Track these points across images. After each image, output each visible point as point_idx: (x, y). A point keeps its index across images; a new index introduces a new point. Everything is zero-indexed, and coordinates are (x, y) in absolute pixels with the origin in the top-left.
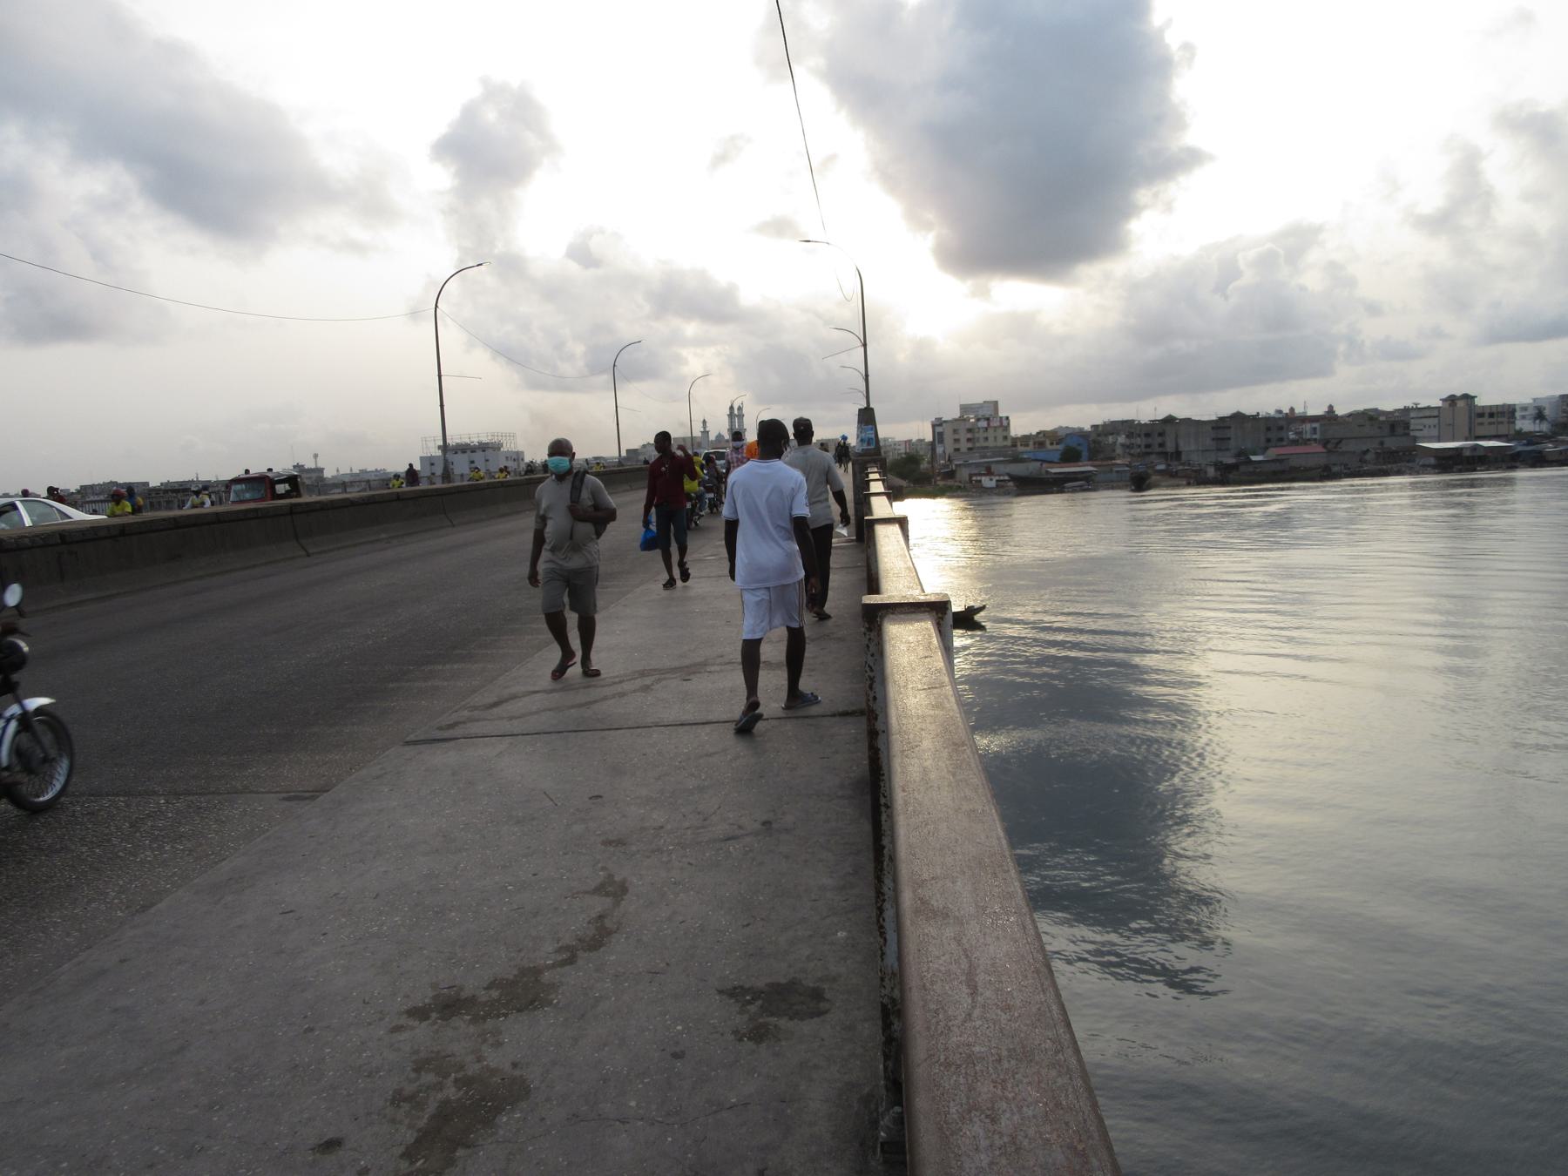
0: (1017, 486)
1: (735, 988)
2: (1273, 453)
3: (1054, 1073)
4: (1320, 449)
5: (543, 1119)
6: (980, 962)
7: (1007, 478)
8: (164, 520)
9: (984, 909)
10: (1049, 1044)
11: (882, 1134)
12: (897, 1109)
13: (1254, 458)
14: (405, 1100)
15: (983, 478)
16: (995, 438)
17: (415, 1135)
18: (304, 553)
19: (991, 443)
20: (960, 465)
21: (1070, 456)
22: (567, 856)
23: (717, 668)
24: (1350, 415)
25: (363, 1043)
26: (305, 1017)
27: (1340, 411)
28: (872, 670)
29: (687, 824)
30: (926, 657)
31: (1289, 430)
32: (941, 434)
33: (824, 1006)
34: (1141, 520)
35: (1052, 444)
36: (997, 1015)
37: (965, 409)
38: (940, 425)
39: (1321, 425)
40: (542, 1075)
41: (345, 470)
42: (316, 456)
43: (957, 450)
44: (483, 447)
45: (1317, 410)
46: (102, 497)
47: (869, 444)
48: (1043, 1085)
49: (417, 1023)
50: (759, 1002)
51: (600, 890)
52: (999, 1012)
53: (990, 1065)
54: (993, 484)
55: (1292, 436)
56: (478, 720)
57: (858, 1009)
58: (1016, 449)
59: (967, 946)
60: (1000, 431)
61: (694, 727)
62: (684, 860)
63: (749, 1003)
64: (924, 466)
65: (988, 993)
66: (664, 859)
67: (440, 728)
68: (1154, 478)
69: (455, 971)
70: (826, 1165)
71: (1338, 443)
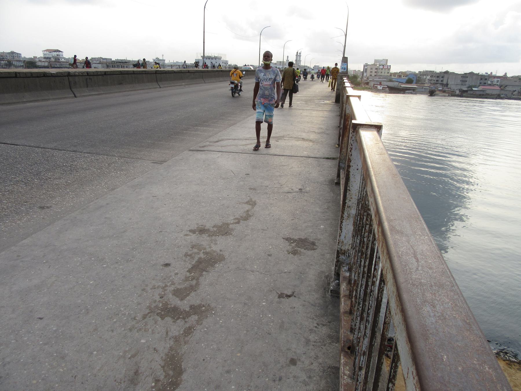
0: (389, 90)
1: (288, 238)
2: (481, 88)
3: (452, 294)
4: (498, 88)
5: (229, 267)
6: (418, 251)
7: (386, 87)
8: (117, 71)
9: (415, 232)
10: (448, 283)
11: (331, 287)
12: (338, 281)
13: (474, 89)
14: (189, 256)
15: (378, 86)
16: (385, 72)
17: (191, 266)
18: (159, 87)
19: (383, 74)
20: (371, 81)
21: (410, 81)
22: (238, 191)
23: (287, 138)
24: (512, 77)
25: (176, 238)
26: (160, 228)
27: (509, 75)
28: (352, 145)
29: (275, 186)
30: (377, 144)
31: (489, 80)
32: (366, 69)
33: (315, 247)
34: (516, 104)
35: (404, 76)
36: (427, 270)
37: (376, 61)
38: (367, 66)
39: (501, 80)
40: (229, 255)
41: (172, 61)
42: (163, 55)
43: (371, 75)
44: (216, 58)
45: (501, 74)
46: (98, 62)
47: (344, 70)
48: (449, 297)
49: (192, 234)
50: (295, 243)
51: (247, 203)
52: (428, 269)
53: (429, 287)
54: (381, 88)
55: (489, 83)
56: (212, 146)
57: (326, 250)
58: (391, 77)
59: (412, 244)
60: (387, 70)
61: (279, 156)
62: (274, 197)
63: (292, 243)
64: (359, 79)
65: (423, 262)
66: (268, 196)
67: (200, 147)
68: (437, 92)
69: (204, 221)
70: (313, 294)
71: (505, 87)
